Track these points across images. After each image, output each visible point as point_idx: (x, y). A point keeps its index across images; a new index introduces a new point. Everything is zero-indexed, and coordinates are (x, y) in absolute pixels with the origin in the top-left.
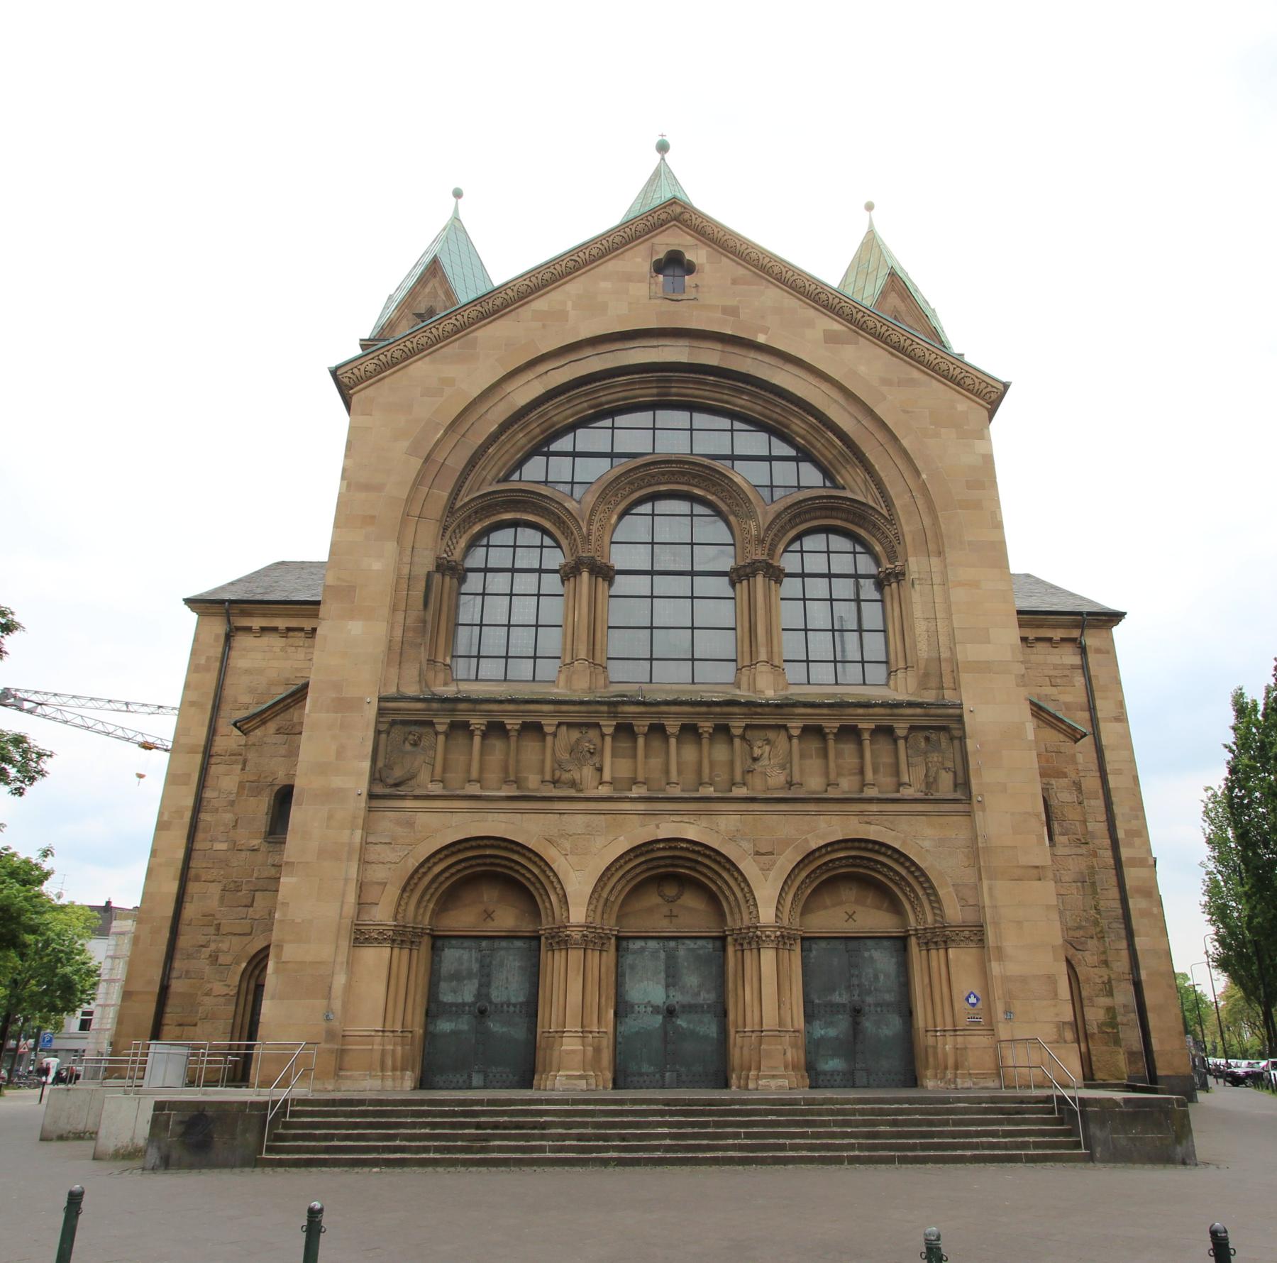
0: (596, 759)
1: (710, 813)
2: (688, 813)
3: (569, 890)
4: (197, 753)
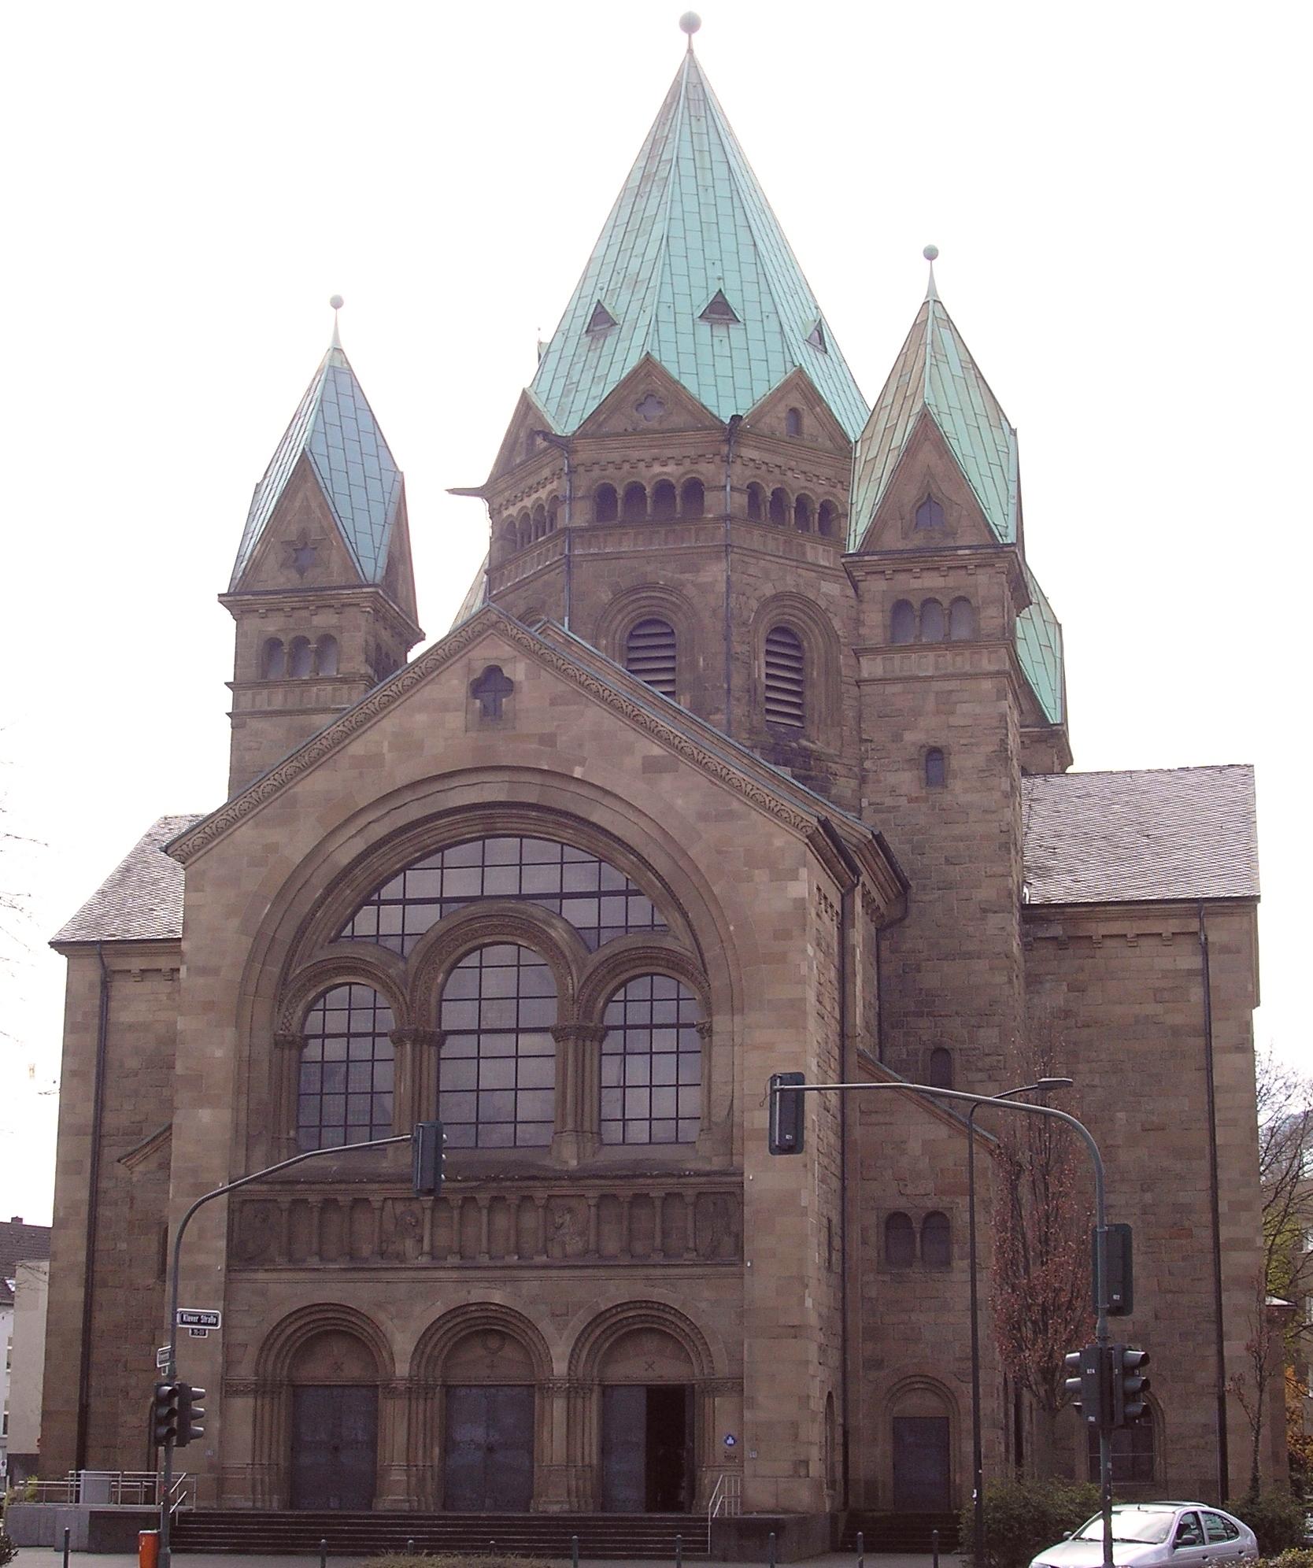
0: (418, 1231)
1: (515, 1280)
2: (494, 1280)
3: (396, 1348)
4: (85, 1134)
